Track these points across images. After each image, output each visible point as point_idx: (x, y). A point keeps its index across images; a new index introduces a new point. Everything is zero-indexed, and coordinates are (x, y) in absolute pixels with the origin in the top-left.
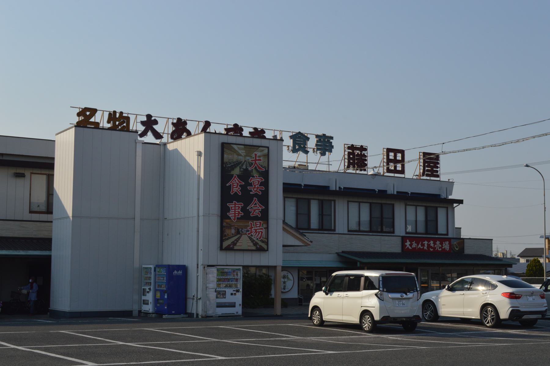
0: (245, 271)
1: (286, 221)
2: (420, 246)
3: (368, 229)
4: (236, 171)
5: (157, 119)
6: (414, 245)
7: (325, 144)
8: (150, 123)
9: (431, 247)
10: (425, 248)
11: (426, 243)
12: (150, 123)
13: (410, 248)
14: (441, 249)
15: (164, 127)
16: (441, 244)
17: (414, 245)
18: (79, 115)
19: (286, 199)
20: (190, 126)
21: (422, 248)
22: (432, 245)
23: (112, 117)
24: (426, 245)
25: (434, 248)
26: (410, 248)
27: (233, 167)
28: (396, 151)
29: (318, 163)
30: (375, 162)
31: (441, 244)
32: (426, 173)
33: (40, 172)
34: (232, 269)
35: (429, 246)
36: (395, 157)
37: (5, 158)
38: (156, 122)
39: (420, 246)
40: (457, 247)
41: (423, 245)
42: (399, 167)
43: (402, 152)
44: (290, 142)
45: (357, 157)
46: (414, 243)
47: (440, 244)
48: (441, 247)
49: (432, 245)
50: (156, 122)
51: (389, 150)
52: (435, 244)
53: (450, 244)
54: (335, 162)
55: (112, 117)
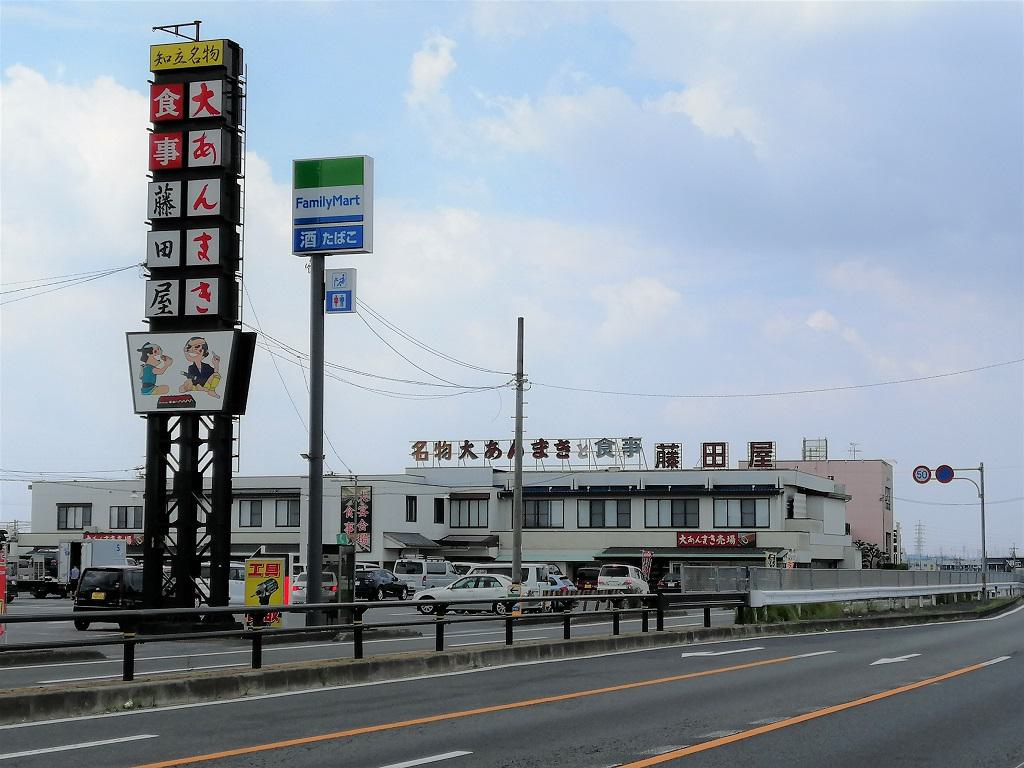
3: (588, 525)
4: (350, 503)
6: (691, 540)
7: (632, 446)
8: (467, 448)
11: (705, 537)
12: (467, 448)
15: (479, 449)
17: (691, 540)
18: (414, 447)
19: (242, 524)
20: (500, 446)
23: (438, 445)
27: (348, 501)
28: (714, 445)
30: (690, 458)
32: (755, 463)
36: (714, 453)
37: (255, 492)
38: (472, 446)
42: (719, 460)
43: (723, 445)
44: (595, 448)
45: (668, 456)
50: (472, 446)
51: (705, 445)
53: (736, 537)
54: (648, 458)
55: (438, 445)
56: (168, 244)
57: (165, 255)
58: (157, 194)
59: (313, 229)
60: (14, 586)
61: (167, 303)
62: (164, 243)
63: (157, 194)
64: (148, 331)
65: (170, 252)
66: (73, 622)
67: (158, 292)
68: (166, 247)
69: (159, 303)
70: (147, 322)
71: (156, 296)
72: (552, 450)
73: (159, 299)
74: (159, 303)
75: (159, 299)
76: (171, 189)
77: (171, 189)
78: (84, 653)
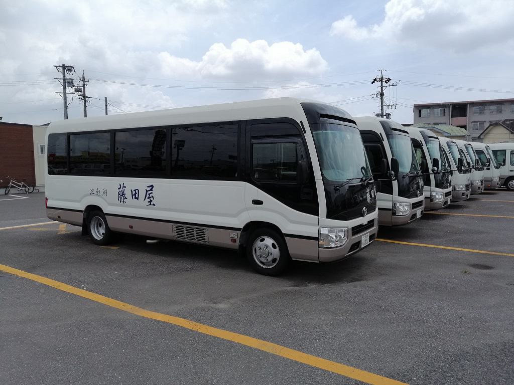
56: (137, 191)
57: (136, 198)
58: (119, 189)
59: (368, 233)
60: (366, 208)
61: (152, 199)
62: (135, 190)
63: (119, 189)
64: (254, 145)
65: (138, 196)
66: (295, 161)
67: (147, 191)
68: (136, 193)
69: (148, 198)
70: (507, 134)
71: (146, 193)
72: (128, 194)
73: (148, 196)
74: (148, 198)
75: (148, 196)
76: (125, 187)
77: (125, 187)
78: (100, 235)
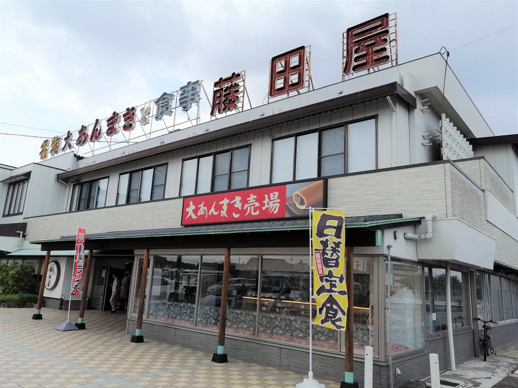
0: (111, 285)
1: (478, 134)
2: (212, 210)
5: (173, 114)
6: (202, 209)
9: (237, 211)
10: (224, 213)
11: (225, 202)
13: (194, 217)
14: (258, 213)
16: (260, 200)
21: (216, 213)
22: (238, 205)
24: (225, 208)
25: (243, 212)
26: (194, 217)
29: (150, 133)
31: (260, 200)
33: (363, 116)
34: (253, 227)
35: (231, 208)
39: (212, 210)
40: (302, 203)
41: (219, 208)
46: (201, 206)
47: (256, 200)
48: (259, 208)
49: (238, 205)
52: (244, 201)
53: (282, 197)
